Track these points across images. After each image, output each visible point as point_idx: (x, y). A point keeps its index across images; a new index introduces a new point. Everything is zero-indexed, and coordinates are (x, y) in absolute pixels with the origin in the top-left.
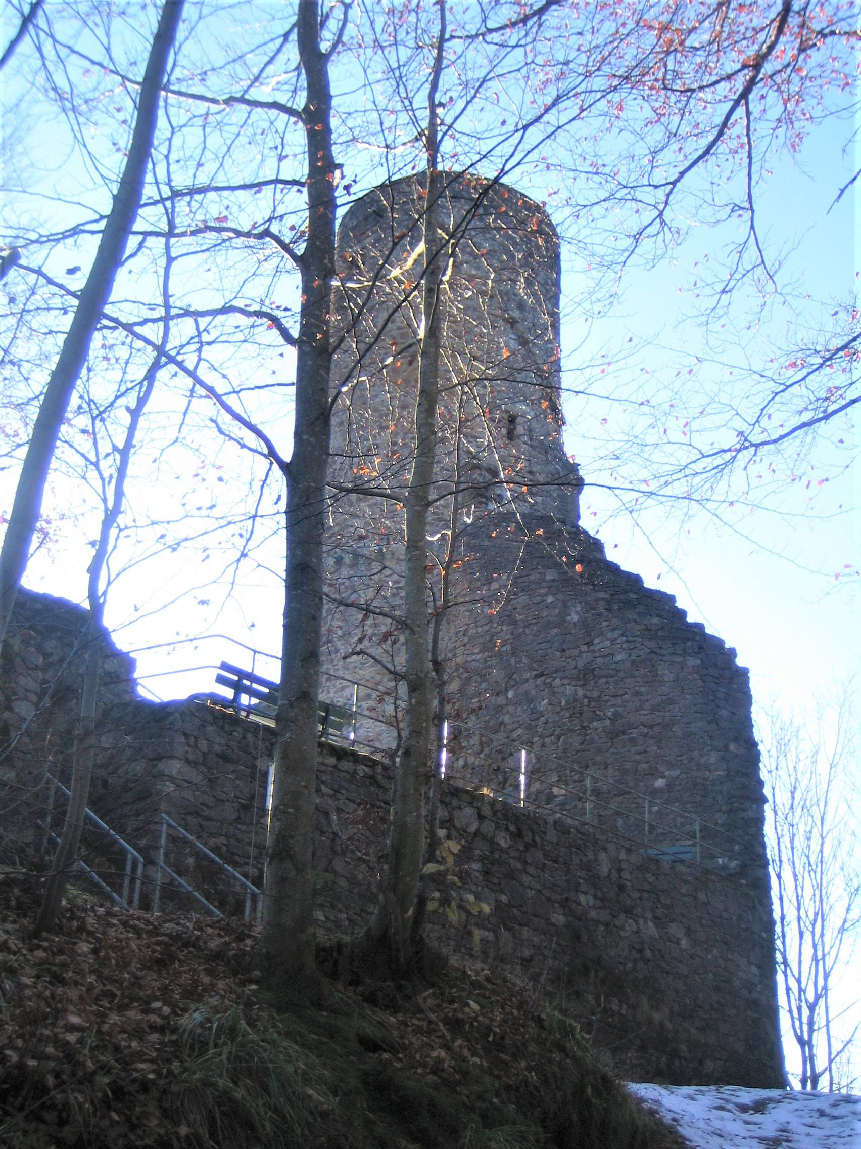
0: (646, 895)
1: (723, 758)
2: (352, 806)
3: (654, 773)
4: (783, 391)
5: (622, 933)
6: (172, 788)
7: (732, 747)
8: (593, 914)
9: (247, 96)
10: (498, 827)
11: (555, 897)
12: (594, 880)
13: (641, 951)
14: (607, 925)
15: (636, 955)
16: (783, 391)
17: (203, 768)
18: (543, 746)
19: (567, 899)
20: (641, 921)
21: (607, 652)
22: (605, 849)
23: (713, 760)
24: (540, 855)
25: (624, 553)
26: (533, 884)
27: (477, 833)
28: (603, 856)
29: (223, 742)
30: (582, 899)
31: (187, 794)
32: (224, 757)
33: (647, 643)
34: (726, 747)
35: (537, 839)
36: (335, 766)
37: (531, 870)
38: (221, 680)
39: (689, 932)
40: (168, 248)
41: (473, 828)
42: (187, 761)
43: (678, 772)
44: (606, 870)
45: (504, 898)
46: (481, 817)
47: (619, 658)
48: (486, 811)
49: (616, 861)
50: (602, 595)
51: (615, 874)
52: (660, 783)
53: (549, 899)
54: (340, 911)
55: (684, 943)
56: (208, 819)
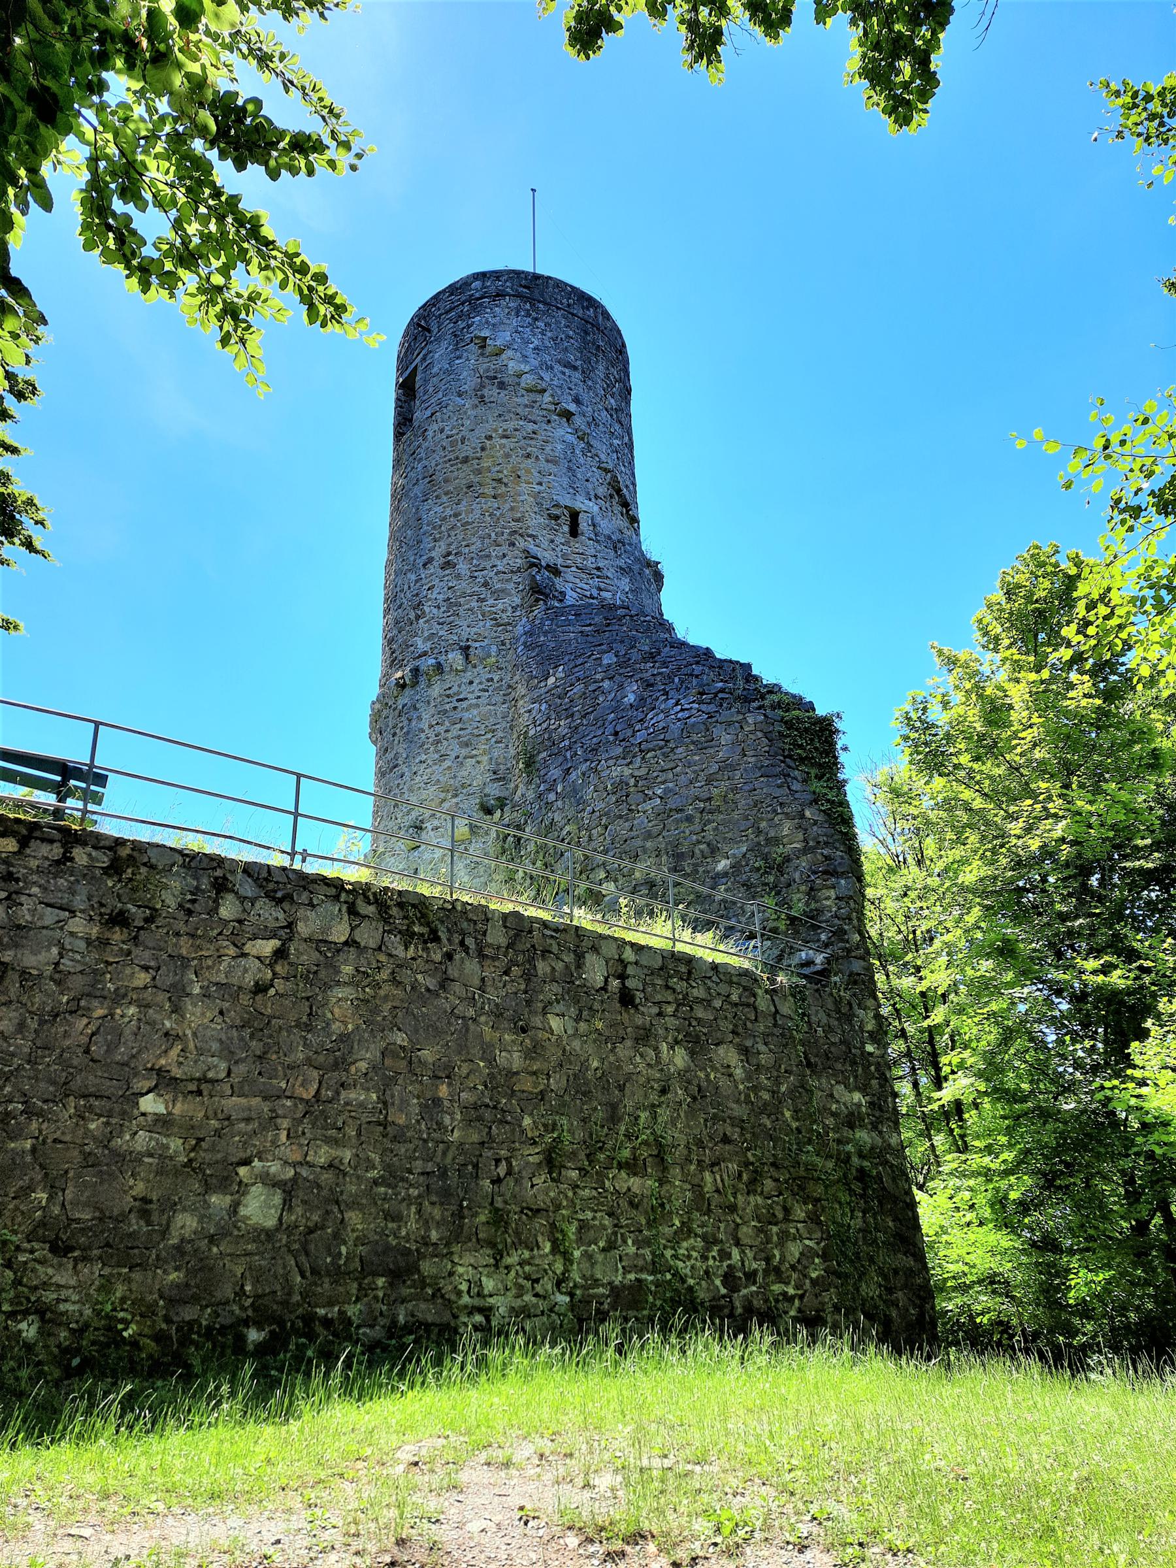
7: (808, 814)
33: (704, 707)
34: (802, 816)
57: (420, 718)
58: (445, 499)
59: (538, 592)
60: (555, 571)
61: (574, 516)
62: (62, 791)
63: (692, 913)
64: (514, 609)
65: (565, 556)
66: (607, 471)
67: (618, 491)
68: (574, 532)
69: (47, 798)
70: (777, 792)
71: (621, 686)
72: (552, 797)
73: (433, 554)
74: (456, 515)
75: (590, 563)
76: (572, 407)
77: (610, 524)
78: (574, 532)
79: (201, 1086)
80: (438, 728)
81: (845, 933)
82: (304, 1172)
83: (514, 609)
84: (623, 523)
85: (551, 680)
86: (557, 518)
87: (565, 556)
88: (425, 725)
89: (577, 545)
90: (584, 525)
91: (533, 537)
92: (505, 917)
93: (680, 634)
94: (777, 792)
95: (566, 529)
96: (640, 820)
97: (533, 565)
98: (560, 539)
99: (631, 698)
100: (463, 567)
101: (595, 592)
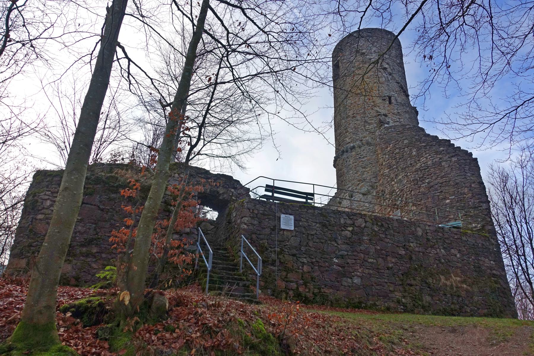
0: (439, 240)
1: (470, 190)
2: (314, 224)
3: (445, 198)
4: (364, 15)
5: (430, 255)
6: (245, 226)
7: (473, 185)
8: (417, 249)
9: (246, 10)
10: (373, 224)
11: (399, 245)
12: (417, 238)
13: (439, 260)
14: (423, 253)
15: (437, 262)
16: (364, 15)
17: (256, 219)
18: (407, 195)
19: (405, 245)
20: (438, 250)
21: (425, 162)
22: (419, 226)
23: (466, 191)
24: (392, 231)
25: (430, 131)
26: (390, 241)
27: (365, 227)
28: (418, 229)
29: (263, 209)
30: (412, 245)
31: (251, 227)
32: (264, 214)
33: (438, 156)
34: (471, 186)
35: (390, 226)
36: (306, 212)
37: (389, 237)
38: (266, 190)
39: (460, 251)
40: (18, 10)
41: (363, 226)
42: (250, 217)
43: (454, 197)
44: (420, 234)
45: (378, 248)
46: (366, 222)
47: (429, 163)
48: (368, 219)
49: (424, 230)
50: (423, 144)
51: (424, 235)
52: (448, 201)
53: (397, 246)
54: (313, 259)
55: (458, 255)
56: (259, 234)
57: (350, 161)
58: (351, 98)
59: (381, 123)
60: (386, 115)
61: (390, 98)
62: (307, 198)
63: (512, 306)
64: (375, 128)
65: (388, 111)
66: (398, 83)
67: (402, 88)
68: (390, 103)
69: (304, 200)
70: (463, 180)
71: (411, 150)
72: (393, 183)
73: (349, 114)
74: (355, 102)
75: (396, 111)
76: (387, 66)
77: (401, 98)
78: (390, 103)
79: (342, 257)
80: (355, 164)
81: (94, 338)
82: (364, 274)
83: (375, 128)
84: (404, 97)
85: (389, 149)
86: (384, 100)
87: (388, 111)
88: (351, 163)
89: (392, 107)
90: (393, 101)
91: (379, 106)
92: (397, 220)
93: (427, 132)
94: (463, 180)
95: (388, 102)
96: (422, 190)
97: (379, 115)
98: (386, 106)
99: (414, 153)
100: (358, 117)
101: (398, 120)
